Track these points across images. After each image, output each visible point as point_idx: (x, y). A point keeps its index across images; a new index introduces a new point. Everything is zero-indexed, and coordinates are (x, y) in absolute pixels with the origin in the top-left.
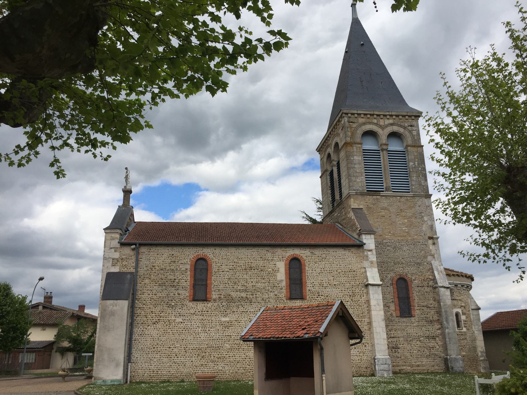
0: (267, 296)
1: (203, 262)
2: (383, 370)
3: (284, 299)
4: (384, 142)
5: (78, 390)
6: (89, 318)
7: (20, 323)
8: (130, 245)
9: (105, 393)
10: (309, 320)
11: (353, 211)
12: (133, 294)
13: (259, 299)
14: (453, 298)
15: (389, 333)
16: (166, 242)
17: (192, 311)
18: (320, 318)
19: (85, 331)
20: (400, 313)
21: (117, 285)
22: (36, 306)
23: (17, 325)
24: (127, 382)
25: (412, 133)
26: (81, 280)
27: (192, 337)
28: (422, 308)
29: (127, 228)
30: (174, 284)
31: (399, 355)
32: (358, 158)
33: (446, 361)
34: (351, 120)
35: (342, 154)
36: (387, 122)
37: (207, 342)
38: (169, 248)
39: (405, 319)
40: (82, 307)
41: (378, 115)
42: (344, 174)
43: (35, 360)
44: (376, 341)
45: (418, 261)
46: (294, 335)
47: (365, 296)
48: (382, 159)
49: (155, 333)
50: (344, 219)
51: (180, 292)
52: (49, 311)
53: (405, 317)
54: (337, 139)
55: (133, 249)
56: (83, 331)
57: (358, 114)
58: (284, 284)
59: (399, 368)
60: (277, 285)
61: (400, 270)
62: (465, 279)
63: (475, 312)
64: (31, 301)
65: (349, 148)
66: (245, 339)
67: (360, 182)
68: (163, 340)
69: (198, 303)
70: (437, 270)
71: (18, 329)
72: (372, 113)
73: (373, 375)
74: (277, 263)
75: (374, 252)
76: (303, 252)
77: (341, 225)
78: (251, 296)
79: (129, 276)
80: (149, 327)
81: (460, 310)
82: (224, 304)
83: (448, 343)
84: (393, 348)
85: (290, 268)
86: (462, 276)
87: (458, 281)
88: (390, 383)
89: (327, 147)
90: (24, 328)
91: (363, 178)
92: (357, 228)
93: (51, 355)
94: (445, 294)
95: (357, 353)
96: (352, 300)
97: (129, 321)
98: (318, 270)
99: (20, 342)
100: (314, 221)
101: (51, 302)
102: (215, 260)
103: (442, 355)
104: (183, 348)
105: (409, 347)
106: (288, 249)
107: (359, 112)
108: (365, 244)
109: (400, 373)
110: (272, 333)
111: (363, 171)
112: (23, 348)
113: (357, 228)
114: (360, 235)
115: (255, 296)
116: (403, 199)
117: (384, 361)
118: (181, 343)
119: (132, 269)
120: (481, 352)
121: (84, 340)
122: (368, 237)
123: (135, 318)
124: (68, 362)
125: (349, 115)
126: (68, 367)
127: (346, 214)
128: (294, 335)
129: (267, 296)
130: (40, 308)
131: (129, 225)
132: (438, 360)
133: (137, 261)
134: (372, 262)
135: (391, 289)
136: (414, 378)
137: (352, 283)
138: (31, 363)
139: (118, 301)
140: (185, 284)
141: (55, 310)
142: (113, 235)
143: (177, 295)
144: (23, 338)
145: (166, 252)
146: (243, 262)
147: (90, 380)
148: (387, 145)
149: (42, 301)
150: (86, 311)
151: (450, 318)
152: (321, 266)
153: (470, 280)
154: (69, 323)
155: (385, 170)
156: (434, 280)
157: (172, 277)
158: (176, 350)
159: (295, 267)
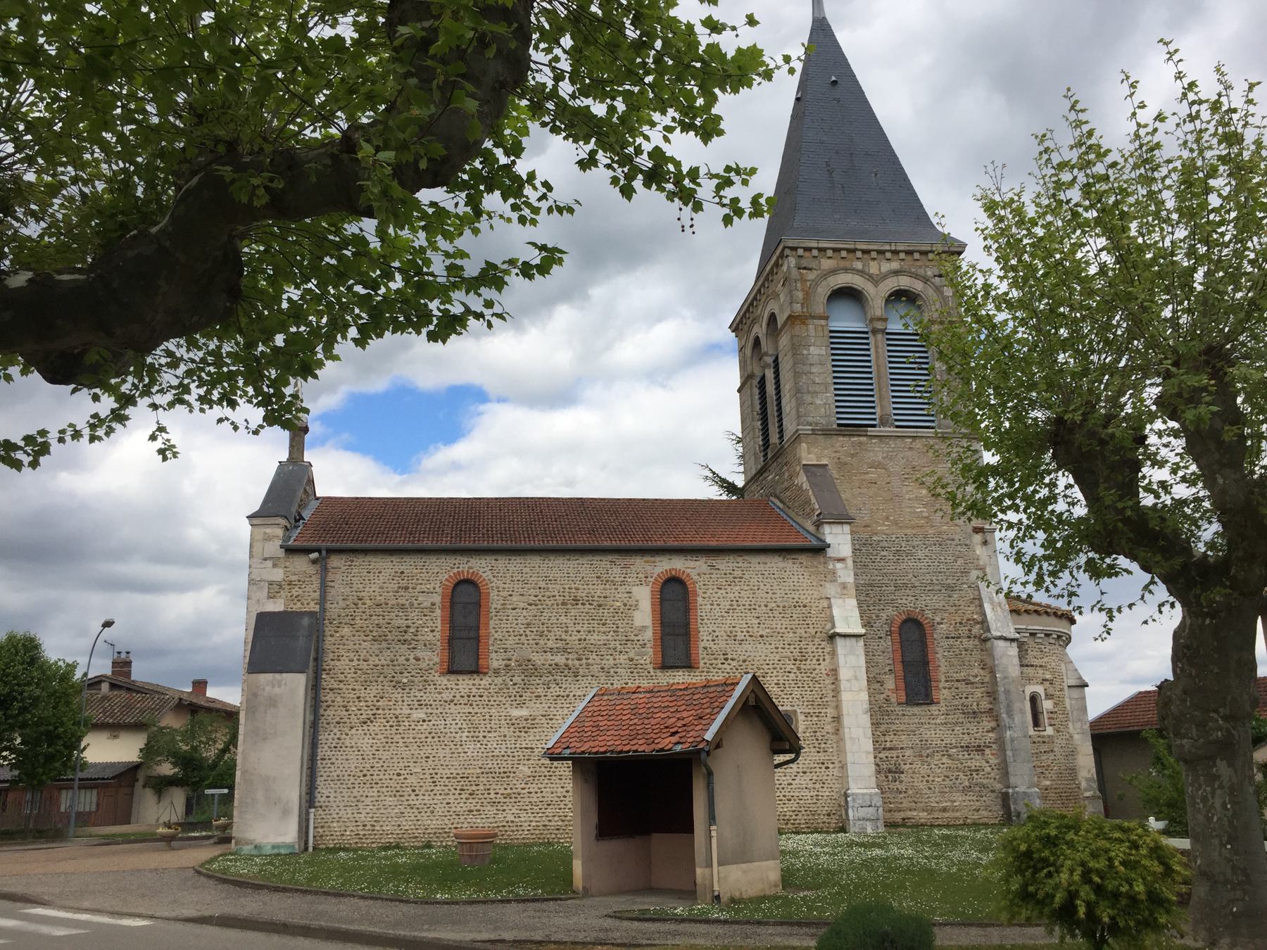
0: (612, 662)
1: (470, 588)
2: (864, 819)
3: (650, 667)
4: (878, 313)
5: (202, 865)
6: (218, 710)
7: (62, 724)
8: (306, 551)
9: (261, 870)
10: (685, 714)
11: (806, 472)
12: (316, 660)
13: (595, 669)
14: (1025, 662)
15: (882, 739)
16: (387, 545)
17: (447, 696)
18: (708, 711)
19: (209, 739)
20: (907, 695)
21: (281, 641)
22: (96, 683)
23: (56, 728)
24: (306, 849)
25: (942, 293)
26: (198, 618)
27: (447, 750)
28: (957, 684)
29: (300, 514)
30: (407, 638)
31: (902, 787)
32: (818, 351)
33: (1005, 798)
34: (804, 263)
35: (784, 341)
36: (886, 267)
37: (480, 763)
38: (393, 558)
39: (916, 710)
40: (200, 685)
41: (865, 252)
42: (787, 387)
43: (98, 805)
44: (850, 758)
45: (949, 581)
46: (653, 746)
47: (828, 661)
48: (872, 352)
49: (365, 743)
50: (787, 489)
51: (420, 655)
52: (123, 693)
53: (918, 704)
54: (773, 306)
55: (314, 562)
56: (204, 739)
57: (820, 249)
58: (649, 634)
59: (903, 815)
60: (633, 637)
61: (907, 602)
62: (1052, 619)
63: (1075, 693)
64: (85, 674)
65: (798, 329)
66: (553, 756)
67: (823, 405)
68: (384, 758)
69: (460, 677)
70: (991, 601)
71: (59, 737)
72: (852, 247)
73: (843, 830)
74: (635, 589)
75: (850, 563)
76: (691, 564)
77: (782, 501)
78: (577, 663)
79: (306, 621)
80: (354, 731)
81: (1040, 690)
82: (517, 679)
83: (1010, 759)
84: (890, 771)
85: (662, 600)
86: (1046, 613)
87: (1038, 624)
88: (874, 845)
89: (754, 321)
90: (73, 735)
91: (830, 396)
92: (813, 510)
93: (132, 794)
94: (1007, 655)
95: (796, 783)
96: (799, 669)
97: (310, 718)
98: (725, 605)
99: (65, 765)
100: (730, 487)
101: (128, 674)
102: (497, 583)
103: (998, 786)
104: (428, 776)
105: (924, 770)
106: (657, 559)
107: (822, 245)
108: (829, 546)
109: (904, 825)
110: (610, 742)
111: (830, 380)
112: (73, 780)
113: (813, 510)
114: (818, 525)
115: (584, 661)
116: (918, 444)
117: (867, 798)
118: (424, 764)
119: (312, 604)
120: (1087, 780)
121: (206, 759)
122: (837, 529)
123: (322, 711)
124: (173, 806)
125: (800, 252)
126: (174, 819)
127: (791, 477)
128: (653, 746)
129: (612, 662)
130: (105, 687)
131: (303, 505)
132: (989, 799)
133: (324, 588)
134: (844, 586)
135: (887, 643)
136: (929, 836)
137: (799, 631)
138: (90, 813)
139: (285, 675)
140: (430, 637)
141: (138, 692)
142: (268, 530)
143: (412, 661)
144: (71, 755)
145: (386, 567)
146: (558, 587)
147: (227, 846)
148: (885, 320)
149: (108, 672)
150: (211, 693)
151: (1017, 706)
152: (731, 595)
153: (1065, 623)
154: (171, 721)
155: (879, 378)
156: (984, 622)
157: (401, 622)
158: (412, 780)
159: (675, 599)
